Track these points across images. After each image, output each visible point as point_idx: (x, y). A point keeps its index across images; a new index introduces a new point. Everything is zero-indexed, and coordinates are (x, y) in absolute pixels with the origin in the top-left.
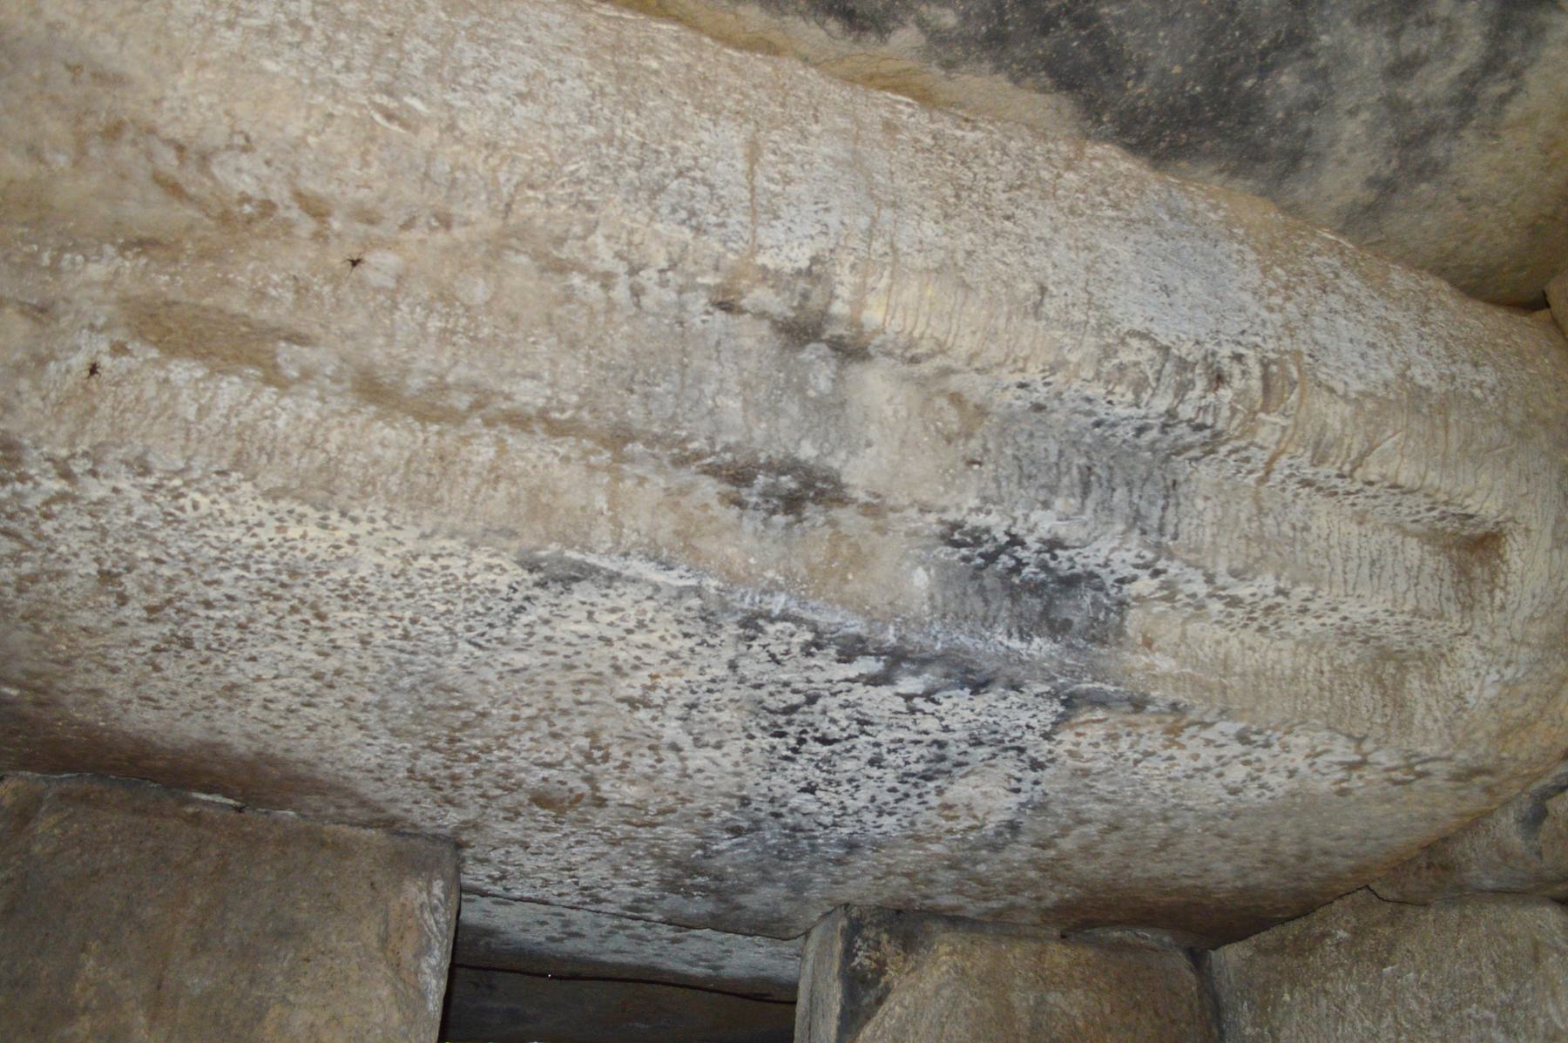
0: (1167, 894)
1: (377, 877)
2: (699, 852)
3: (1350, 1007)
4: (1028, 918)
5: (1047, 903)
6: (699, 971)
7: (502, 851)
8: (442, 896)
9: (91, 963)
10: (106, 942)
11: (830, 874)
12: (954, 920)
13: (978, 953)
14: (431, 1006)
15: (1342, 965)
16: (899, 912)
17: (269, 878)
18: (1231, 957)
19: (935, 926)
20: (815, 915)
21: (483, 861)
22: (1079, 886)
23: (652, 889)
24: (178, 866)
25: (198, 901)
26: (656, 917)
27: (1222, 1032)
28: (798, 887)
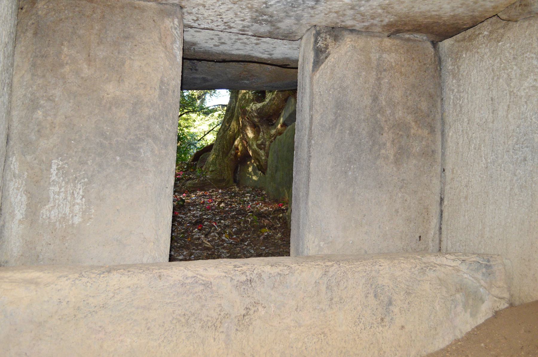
0: (426, 18)
1: (155, 18)
2: (264, 5)
3: (485, 57)
4: (378, 29)
5: (384, 23)
6: (265, 56)
7: (196, 9)
8: (178, 24)
9: (66, 49)
10: (69, 42)
11: (309, 13)
12: (352, 31)
13: (360, 41)
14: (178, 60)
15: (484, 43)
16: (333, 28)
17: (119, 19)
18: (446, 44)
19: (346, 33)
20: (304, 30)
21: (190, 13)
22: (395, 16)
23: (249, 22)
24: (88, 17)
25: (97, 28)
26: (250, 33)
27: (441, 69)
28: (298, 19)
